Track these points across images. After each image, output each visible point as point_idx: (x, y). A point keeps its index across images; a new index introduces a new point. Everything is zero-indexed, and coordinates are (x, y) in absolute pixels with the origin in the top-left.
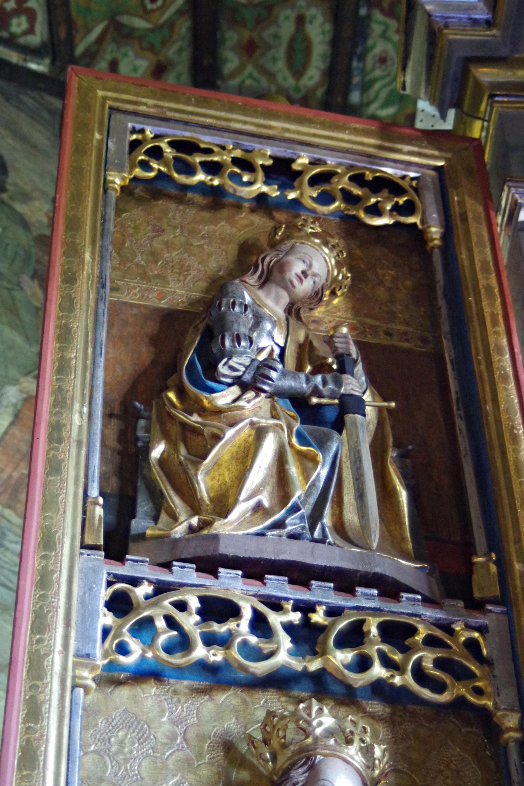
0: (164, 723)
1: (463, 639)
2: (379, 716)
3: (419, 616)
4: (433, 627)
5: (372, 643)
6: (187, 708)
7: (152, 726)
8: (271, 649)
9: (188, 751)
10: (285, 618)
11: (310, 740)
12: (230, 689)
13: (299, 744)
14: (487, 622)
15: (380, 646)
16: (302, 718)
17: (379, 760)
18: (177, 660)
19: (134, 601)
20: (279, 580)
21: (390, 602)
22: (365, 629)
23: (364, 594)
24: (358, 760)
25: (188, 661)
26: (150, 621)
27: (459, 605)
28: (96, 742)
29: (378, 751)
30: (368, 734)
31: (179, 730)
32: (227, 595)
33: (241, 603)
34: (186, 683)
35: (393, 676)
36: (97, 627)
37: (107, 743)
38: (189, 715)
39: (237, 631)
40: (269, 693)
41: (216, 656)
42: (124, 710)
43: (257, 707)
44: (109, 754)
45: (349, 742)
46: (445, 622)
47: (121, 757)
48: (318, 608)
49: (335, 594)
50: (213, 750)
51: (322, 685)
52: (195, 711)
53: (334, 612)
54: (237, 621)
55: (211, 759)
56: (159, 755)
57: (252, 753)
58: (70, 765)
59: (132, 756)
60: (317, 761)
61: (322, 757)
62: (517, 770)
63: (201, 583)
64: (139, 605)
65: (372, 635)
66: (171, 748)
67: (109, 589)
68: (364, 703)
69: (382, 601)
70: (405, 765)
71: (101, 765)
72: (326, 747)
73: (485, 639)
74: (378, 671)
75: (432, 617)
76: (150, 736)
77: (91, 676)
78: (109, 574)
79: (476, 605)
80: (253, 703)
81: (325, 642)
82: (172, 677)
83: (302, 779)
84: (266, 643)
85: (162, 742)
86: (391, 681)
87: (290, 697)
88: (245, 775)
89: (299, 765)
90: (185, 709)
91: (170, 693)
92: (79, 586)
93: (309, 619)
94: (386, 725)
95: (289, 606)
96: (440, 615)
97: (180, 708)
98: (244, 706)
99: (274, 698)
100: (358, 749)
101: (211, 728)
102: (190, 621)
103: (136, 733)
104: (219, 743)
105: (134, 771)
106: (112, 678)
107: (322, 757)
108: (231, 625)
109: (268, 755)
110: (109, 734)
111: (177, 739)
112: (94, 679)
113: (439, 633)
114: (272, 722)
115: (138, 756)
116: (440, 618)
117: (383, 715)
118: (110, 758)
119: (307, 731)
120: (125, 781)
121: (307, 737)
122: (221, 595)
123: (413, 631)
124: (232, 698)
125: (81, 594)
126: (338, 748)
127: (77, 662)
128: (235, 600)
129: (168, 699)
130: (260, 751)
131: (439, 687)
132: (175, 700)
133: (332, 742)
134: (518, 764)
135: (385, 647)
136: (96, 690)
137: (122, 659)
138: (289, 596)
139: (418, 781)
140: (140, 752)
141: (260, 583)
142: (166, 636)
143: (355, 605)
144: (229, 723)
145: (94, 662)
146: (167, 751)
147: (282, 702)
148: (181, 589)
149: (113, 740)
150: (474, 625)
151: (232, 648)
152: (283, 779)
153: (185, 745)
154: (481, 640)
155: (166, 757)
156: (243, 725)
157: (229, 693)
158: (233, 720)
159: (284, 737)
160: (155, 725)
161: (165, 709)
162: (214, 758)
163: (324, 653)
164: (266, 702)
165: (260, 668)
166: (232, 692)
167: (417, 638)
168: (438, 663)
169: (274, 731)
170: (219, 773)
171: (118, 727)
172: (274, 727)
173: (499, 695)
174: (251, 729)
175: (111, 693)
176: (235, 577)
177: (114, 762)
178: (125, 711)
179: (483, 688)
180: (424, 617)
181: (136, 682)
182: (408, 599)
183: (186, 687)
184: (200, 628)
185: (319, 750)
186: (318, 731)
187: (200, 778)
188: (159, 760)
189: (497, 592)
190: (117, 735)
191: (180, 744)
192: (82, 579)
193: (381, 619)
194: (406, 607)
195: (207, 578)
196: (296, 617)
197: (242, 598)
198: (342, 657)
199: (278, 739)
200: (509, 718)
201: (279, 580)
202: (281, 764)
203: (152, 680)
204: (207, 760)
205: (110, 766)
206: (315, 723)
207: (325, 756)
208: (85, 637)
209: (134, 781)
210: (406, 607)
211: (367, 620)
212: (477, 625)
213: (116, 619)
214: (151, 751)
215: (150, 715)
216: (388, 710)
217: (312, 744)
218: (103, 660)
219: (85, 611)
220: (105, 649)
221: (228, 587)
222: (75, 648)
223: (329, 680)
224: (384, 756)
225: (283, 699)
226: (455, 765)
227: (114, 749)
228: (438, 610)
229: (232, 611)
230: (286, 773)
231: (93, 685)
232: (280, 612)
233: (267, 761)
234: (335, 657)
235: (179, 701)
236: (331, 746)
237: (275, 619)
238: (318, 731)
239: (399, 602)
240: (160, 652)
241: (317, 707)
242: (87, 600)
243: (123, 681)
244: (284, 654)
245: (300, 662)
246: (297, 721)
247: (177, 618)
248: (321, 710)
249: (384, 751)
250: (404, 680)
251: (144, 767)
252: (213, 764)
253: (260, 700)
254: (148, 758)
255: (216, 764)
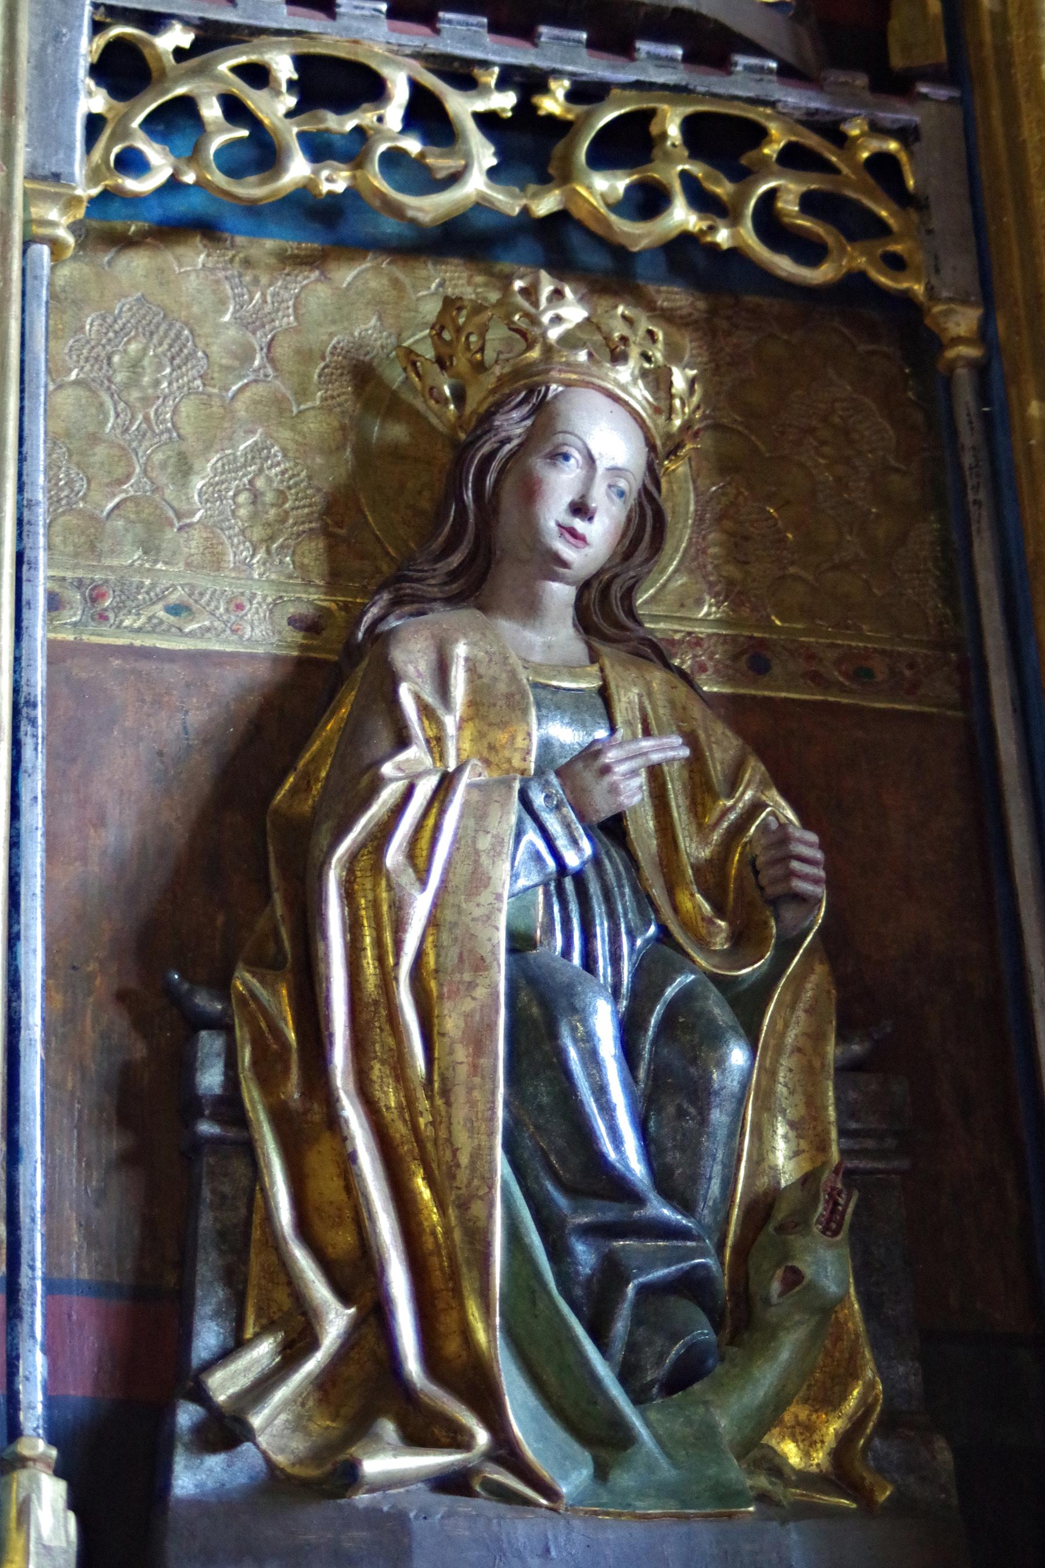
0: (226, 326)
1: (865, 155)
2: (681, 317)
3: (772, 104)
4: (800, 128)
5: (669, 158)
6: (273, 295)
7: (198, 331)
8: (452, 170)
9: (278, 382)
10: (481, 105)
11: (535, 354)
12: (364, 258)
13: (512, 362)
14: (917, 119)
15: (687, 167)
16: (518, 309)
17: (681, 399)
18: (251, 189)
19: (152, 64)
20: (467, 24)
21: (708, 74)
22: (654, 129)
23: (653, 57)
24: (640, 395)
25: (273, 193)
26: (187, 106)
27: (858, 82)
28: (82, 363)
29: (679, 381)
30: (660, 345)
31: (259, 340)
32: (356, 53)
33: (386, 71)
34: (269, 244)
35: (712, 229)
36: (74, 118)
37: (105, 367)
38: (278, 310)
39: (378, 131)
40: (449, 268)
41: (335, 181)
42: (137, 300)
43: (423, 296)
44: (109, 388)
45: (618, 357)
46: (828, 118)
47: (135, 394)
48: (553, 85)
49: (590, 55)
50: (330, 382)
51: (559, 244)
52: (291, 303)
53: (586, 93)
54: (377, 108)
55: (326, 399)
56: (216, 391)
57: (413, 388)
58: (26, 403)
59: (159, 392)
60: (550, 395)
61: (560, 389)
62: (971, 422)
63: (299, 28)
64: (163, 73)
65: (669, 143)
66: (241, 377)
67: (96, 39)
68: (651, 289)
69: (691, 72)
70: (738, 418)
71: (93, 411)
72: (571, 366)
73: (911, 155)
74: (682, 216)
75: (799, 108)
76: (195, 352)
77: (65, 221)
78: (96, 6)
79: (894, 84)
80: (414, 286)
81: (568, 158)
82: (239, 232)
83: (519, 431)
84: (442, 156)
85: (221, 366)
86: (709, 239)
87: (491, 274)
88: (398, 432)
89: (513, 403)
90: (269, 299)
91: (236, 264)
92: (31, 30)
93: (535, 108)
94: (699, 334)
95: (491, 78)
96: (815, 102)
97: (258, 295)
98: (394, 293)
99: (459, 278)
100: (637, 372)
101: (325, 338)
102: (275, 107)
103: (165, 346)
104: (343, 367)
105: (164, 421)
106: (112, 227)
107: (560, 389)
108: (366, 117)
109: (447, 391)
110: (108, 348)
111: (253, 359)
112: (73, 228)
113: (812, 141)
114: (454, 320)
115: (171, 393)
116: (817, 110)
117: (690, 315)
118: (112, 396)
119: (529, 336)
120: (146, 443)
121: (530, 347)
122: (342, 54)
123: (759, 134)
124: (368, 276)
125: (36, 47)
126: (594, 369)
127: (32, 190)
128: (374, 65)
129: (233, 276)
130: (429, 382)
131: (809, 251)
132: (247, 278)
133: (582, 356)
134: (973, 410)
135: (697, 169)
136: (75, 257)
137: (132, 184)
138: (491, 57)
139: (762, 448)
140: (175, 385)
141: (426, 30)
142: (222, 135)
143: (633, 78)
144: (363, 327)
145: (70, 192)
146: (234, 384)
147: (477, 286)
148: (256, 41)
149: (116, 359)
150: (888, 125)
151: (369, 167)
152: (479, 432)
153: (270, 371)
154: (903, 157)
155: (230, 394)
156: (393, 330)
157: (364, 266)
158: (373, 321)
159: (482, 350)
160: (207, 329)
161: (228, 298)
162: (333, 397)
163: (567, 177)
164: (441, 285)
165: (429, 207)
166: (368, 265)
167: (766, 151)
168: (809, 203)
169: (458, 339)
170: (343, 428)
171: (127, 335)
172: (458, 330)
173: (937, 271)
174: (411, 340)
175: (109, 263)
176: (373, 16)
177: (122, 405)
178: (142, 300)
179: (906, 256)
180: (782, 108)
181: (162, 241)
182: (748, 68)
183: (271, 253)
184: (298, 125)
185: (554, 374)
186: (554, 334)
187: (305, 437)
188: (216, 402)
189: (941, 54)
190: (125, 351)
191: (260, 368)
192: (37, 16)
193: (690, 110)
194: (742, 84)
195: (310, 18)
196: (505, 102)
197: (388, 61)
198: (606, 186)
199: (468, 355)
200: (958, 318)
201: (467, 24)
202: (475, 406)
203: (198, 238)
204: (318, 403)
205: (112, 413)
206: (545, 319)
207: (568, 384)
208: (50, 135)
209: (166, 444)
210: (742, 84)
211: (659, 113)
212: (895, 126)
213: (114, 102)
214: (198, 382)
215: (195, 309)
216: (701, 305)
217: (541, 361)
218: (89, 188)
219: (46, 84)
220: (93, 164)
221: (357, 37)
222: (27, 161)
223: (576, 239)
224: (691, 390)
225: (479, 279)
226: (841, 417)
227: (119, 378)
228: (811, 93)
229: (362, 85)
230: (486, 420)
231: (71, 240)
232: (470, 93)
233: (446, 402)
234: (589, 188)
235: (256, 281)
236: (579, 365)
237: (461, 106)
238: (554, 334)
239: (730, 73)
240: (211, 173)
241: (551, 288)
242: (50, 59)
243: (136, 239)
244: (477, 177)
245: (514, 196)
246: (509, 316)
247: (250, 104)
248: (558, 294)
249: (692, 382)
250: (734, 236)
251: (184, 414)
252: (330, 410)
253: (428, 280)
254: (192, 397)
255: (338, 409)
